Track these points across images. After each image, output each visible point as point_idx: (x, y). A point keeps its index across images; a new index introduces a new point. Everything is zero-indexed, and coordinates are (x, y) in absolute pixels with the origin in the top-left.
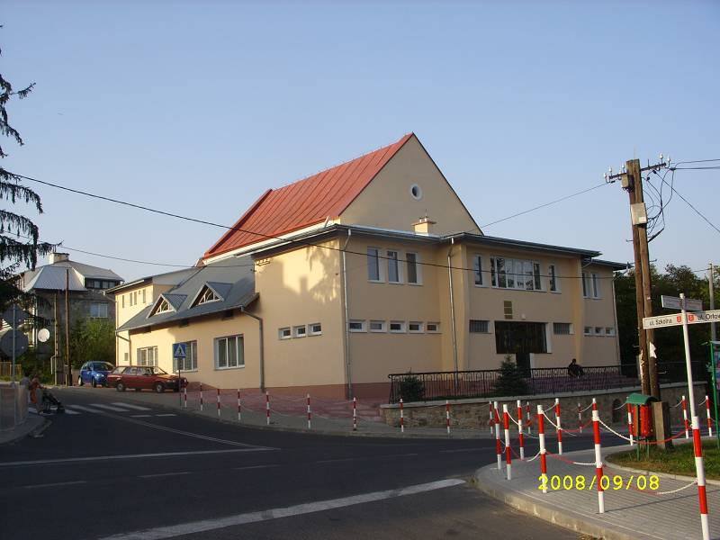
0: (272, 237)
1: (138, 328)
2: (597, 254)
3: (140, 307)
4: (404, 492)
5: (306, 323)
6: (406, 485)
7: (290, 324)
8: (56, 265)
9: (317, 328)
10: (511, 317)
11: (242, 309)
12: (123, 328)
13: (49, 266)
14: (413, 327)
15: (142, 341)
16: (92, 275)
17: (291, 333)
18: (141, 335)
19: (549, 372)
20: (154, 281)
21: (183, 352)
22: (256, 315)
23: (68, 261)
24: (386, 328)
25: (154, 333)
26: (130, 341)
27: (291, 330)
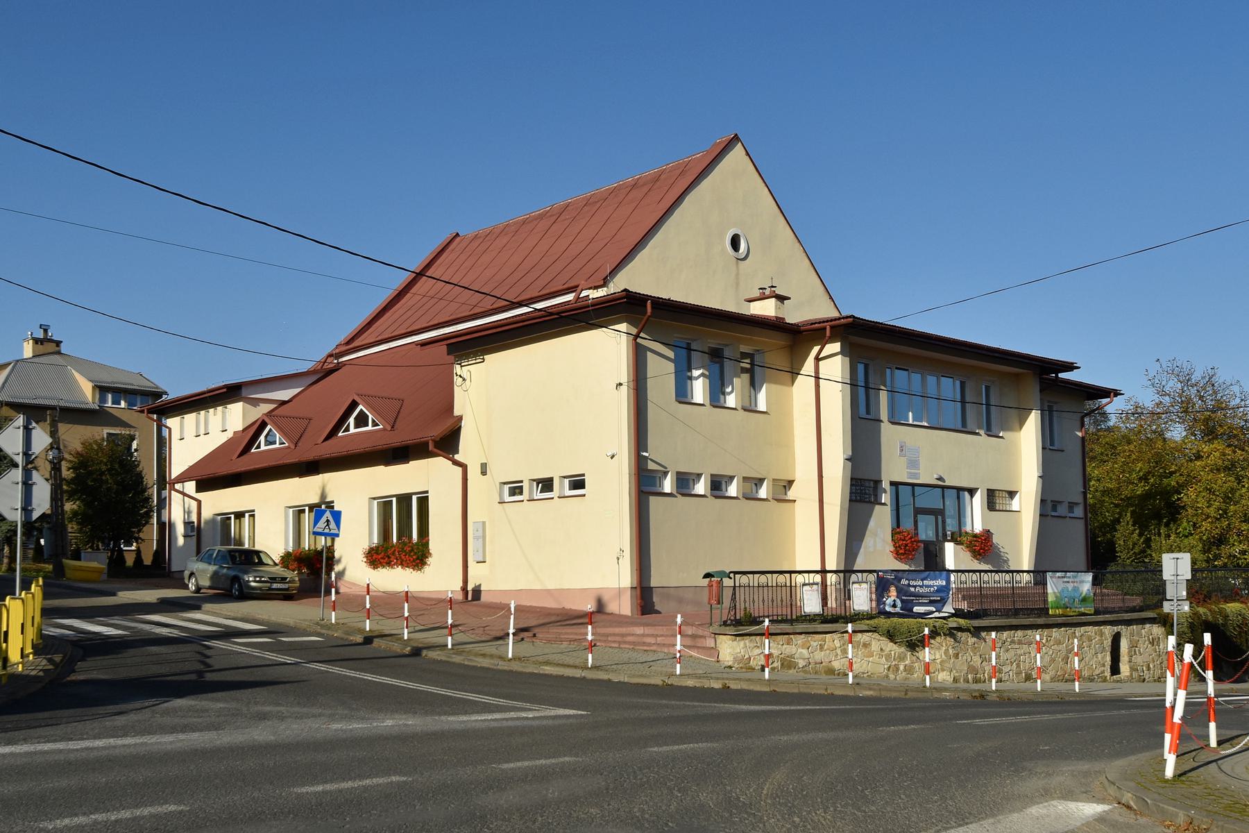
0: (520, 304)
1: (211, 477)
2: (1070, 367)
3: (216, 439)
4: (59, 823)
5: (557, 470)
6: (61, 816)
7: (526, 473)
8: (36, 360)
9: (578, 483)
10: (916, 476)
11: (431, 447)
12: (183, 478)
13: (23, 360)
14: (717, 485)
15: (219, 502)
16: (107, 379)
17: (526, 490)
18: (296, 481)
19: (975, 577)
20: (244, 392)
21: (333, 525)
22: (457, 457)
23: (59, 353)
24: (701, 487)
25: (416, 466)
26: (199, 502)
27: (526, 486)
